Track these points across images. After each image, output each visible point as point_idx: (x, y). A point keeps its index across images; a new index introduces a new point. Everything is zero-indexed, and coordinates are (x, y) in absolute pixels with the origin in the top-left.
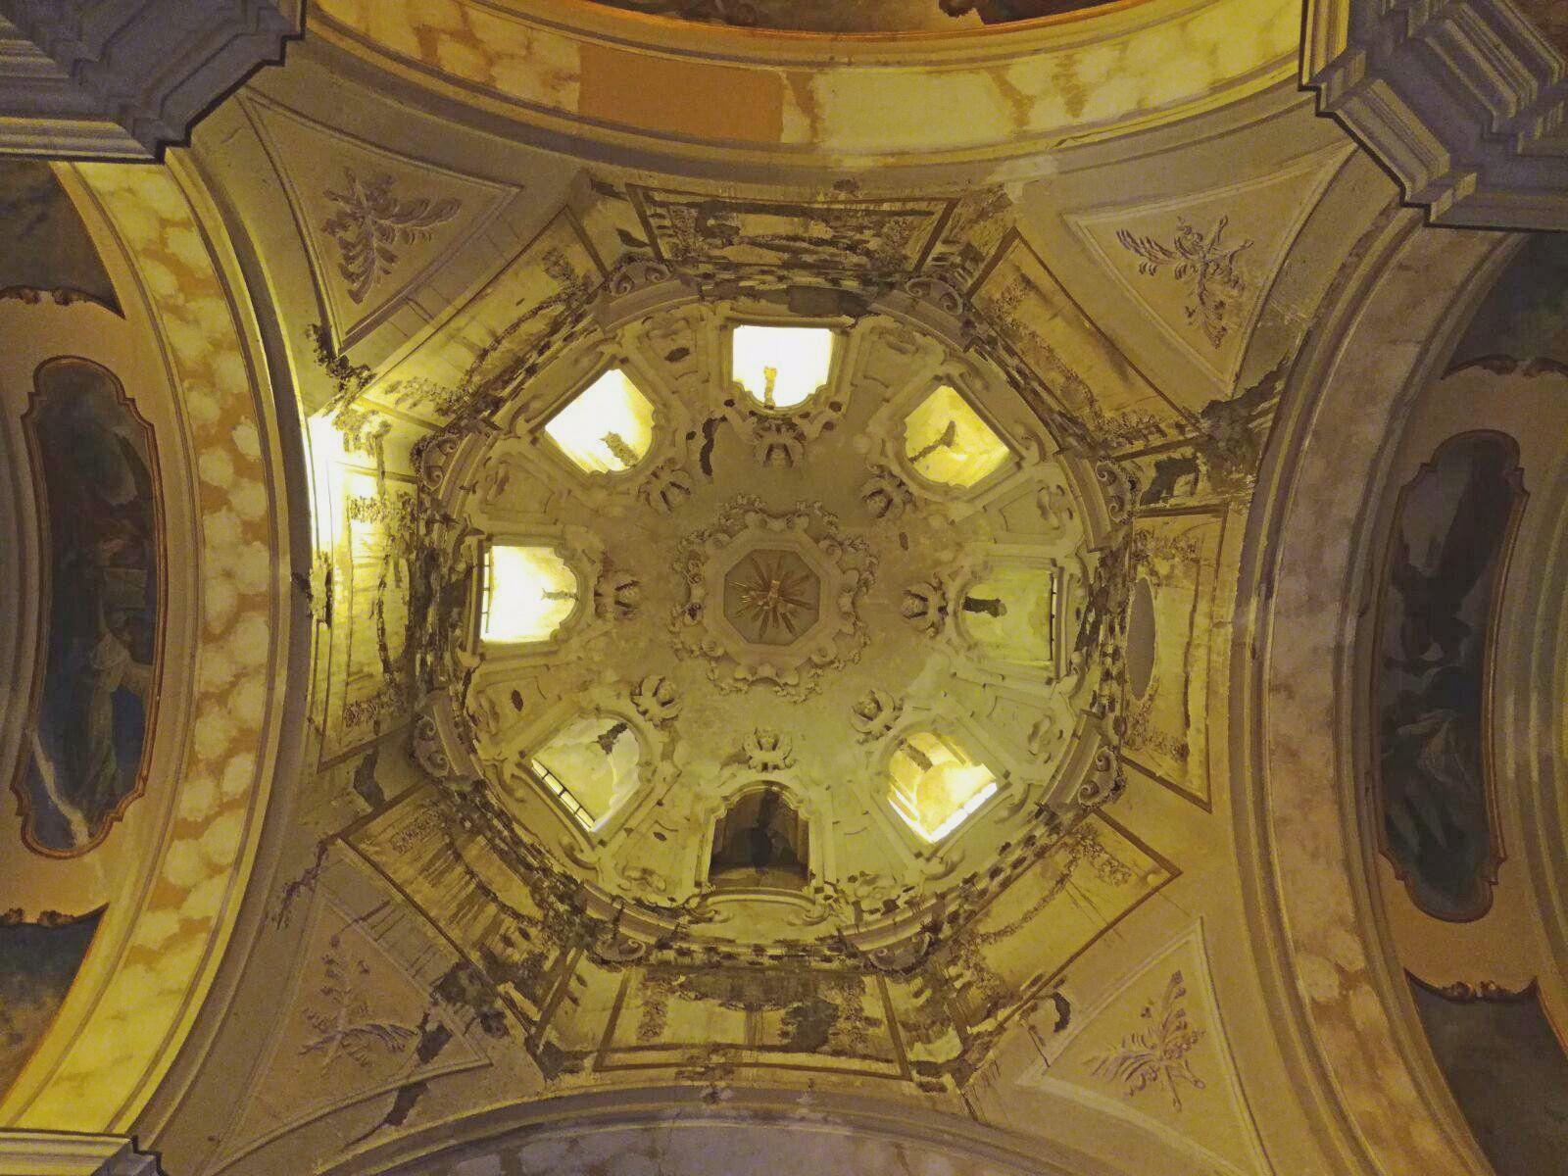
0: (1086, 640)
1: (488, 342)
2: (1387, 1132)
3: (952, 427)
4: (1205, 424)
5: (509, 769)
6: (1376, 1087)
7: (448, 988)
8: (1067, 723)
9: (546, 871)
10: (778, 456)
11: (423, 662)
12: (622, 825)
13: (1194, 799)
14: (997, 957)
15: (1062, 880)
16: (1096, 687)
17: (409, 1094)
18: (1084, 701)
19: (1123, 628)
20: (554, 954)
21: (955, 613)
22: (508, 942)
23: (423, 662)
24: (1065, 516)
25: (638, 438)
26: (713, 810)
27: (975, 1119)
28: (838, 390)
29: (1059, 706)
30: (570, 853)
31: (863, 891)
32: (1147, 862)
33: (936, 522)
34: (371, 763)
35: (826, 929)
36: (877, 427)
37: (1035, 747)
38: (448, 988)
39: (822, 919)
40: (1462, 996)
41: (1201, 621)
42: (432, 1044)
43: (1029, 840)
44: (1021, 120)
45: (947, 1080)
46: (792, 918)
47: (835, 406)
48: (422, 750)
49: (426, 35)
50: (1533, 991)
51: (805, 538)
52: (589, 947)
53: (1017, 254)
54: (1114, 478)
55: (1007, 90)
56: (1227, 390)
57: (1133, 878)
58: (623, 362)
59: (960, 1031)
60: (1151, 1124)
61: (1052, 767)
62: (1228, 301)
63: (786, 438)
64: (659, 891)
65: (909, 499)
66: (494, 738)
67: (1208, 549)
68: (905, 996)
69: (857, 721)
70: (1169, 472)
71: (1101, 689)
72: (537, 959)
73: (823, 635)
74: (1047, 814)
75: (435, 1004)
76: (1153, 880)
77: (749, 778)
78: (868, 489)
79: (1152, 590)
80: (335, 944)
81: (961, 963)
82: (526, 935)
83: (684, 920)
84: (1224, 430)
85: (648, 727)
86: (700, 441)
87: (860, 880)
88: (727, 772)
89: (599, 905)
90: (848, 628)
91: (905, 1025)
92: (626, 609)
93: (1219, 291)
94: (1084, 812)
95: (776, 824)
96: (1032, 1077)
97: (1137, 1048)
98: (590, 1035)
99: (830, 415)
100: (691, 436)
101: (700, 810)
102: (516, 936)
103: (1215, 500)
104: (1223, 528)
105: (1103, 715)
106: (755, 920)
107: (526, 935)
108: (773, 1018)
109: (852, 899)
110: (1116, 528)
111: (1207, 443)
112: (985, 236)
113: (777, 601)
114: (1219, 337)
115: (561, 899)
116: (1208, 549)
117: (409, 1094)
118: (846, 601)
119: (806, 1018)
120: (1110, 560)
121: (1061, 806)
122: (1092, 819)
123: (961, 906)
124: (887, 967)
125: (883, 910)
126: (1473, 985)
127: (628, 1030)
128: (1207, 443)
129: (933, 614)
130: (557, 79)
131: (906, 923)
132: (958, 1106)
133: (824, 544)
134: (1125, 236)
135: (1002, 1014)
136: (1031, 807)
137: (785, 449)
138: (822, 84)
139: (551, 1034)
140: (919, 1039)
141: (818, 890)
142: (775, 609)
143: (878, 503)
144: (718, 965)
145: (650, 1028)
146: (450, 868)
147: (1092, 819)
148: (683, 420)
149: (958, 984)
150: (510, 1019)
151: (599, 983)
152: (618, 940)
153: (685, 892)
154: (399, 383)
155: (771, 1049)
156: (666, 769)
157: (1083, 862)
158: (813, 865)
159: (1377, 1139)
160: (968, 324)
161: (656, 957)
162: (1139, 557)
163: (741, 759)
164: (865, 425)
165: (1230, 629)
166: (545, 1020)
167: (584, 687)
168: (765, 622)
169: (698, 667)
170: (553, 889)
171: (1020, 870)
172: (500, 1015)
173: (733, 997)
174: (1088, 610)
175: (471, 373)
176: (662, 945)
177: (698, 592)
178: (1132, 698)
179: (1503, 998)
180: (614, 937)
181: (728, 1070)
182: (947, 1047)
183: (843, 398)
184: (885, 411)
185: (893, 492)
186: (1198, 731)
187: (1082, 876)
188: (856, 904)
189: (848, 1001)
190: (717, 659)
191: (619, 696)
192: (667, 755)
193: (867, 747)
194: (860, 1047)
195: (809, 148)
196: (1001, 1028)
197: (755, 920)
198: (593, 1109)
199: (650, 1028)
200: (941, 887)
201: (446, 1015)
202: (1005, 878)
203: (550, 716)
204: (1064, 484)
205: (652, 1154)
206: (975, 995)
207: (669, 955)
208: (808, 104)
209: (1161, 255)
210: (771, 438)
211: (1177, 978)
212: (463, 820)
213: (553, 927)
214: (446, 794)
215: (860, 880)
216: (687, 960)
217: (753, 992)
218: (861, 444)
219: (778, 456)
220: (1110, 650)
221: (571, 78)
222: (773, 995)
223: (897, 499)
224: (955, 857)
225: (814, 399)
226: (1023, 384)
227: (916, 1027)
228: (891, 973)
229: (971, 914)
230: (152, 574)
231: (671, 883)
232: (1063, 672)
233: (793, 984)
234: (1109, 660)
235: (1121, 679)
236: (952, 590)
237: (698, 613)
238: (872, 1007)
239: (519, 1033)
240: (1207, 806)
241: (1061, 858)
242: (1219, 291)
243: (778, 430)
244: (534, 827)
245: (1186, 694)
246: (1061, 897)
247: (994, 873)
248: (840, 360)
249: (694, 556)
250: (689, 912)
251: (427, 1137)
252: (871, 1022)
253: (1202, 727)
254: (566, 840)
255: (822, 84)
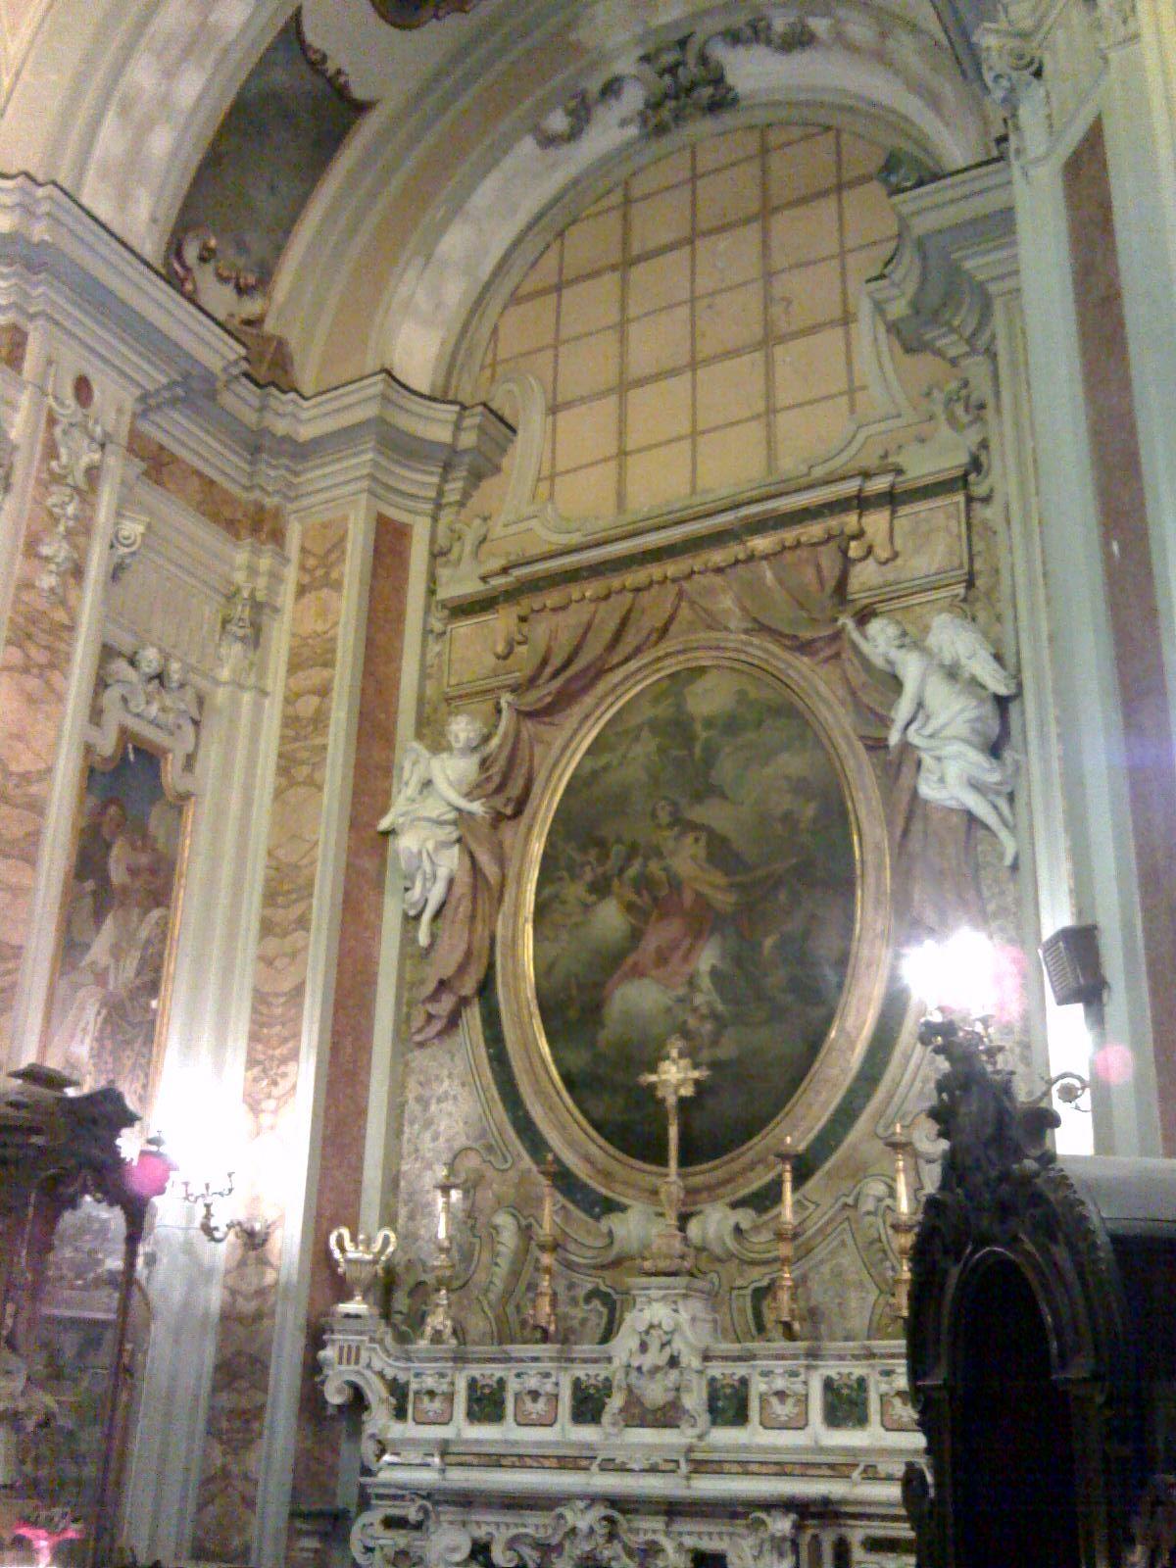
2: (137, 113)
6: (169, 74)
40: (316, 64)
50: (361, 108)
126: (331, 67)
154: (434, 882)
159: (125, 110)
179: (341, 93)
230: (581, 568)
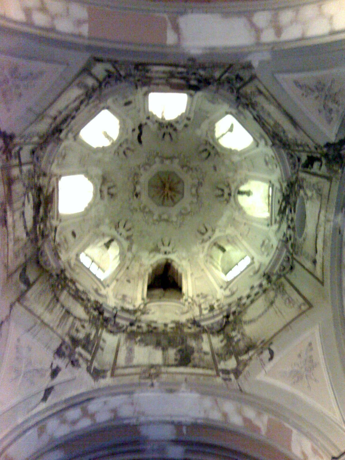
0: (282, 212)
1: (57, 114)
3: (232, 126)
4: (325, 150)
5: (73, 262)
7: (59, 353)
8: (275, 242)
9: (89, 300)
10: (167, 137)
11: (40, 228)
12: (114, 278)
13: (317, 278)
14: (249, 330)
15: (272, 303)
16: (285, 231)
17: (48, 391)
18: (280, 235)
19: (295, 211)
20: (94, 332)
21: (234, 196)
22: (77, 331)
23: (40, 228)
24: (275, 167)
25: (115, 134)
26: (147, 270)
27: (241, 390)
28: (189, 113)
29: (272, 235)
30: (96, 291)
31: (202, 301)
32: (301, 300)
33: (227, 162)
34: (24, 270)
35: (189, 316)
36: (204, 126)
37: (263, 249)
38: (59, 353)
39: (187, 312)
41: (322, 218)
42: (55, 373)
43: (261, 285)
44: (258, 38)
45: (232, 376)
46: (177, 311)
47: (188, 119)
48: (42, 260)
49: (28, 12)
51: (179, 168)
52: (106, 327)
53: (256, 82)
54: (292, 156)
55: (253, 25)
56: (333, 139)
57: (296, 306)
58: (108, 108)
59: (237, 358)
60: (301, 395)
61: (270, 258)
62: (334, 109)
63: (170, 130)
64: (129, 303)
65: (217, 153)
66: (67, 250)
67: (325, 191)
68: (218, 342)
69: (199, 235)
70: (311, 161)
71: (287, 231)
72: (88, 336)
73: (186, 202)
74: (268, 277)
75: (55, 358)
76: (303, 308)
77: (159, 258)
78: (201, 149)
79: (305, 201)
80: (18, 340)
81: (237, 331)
82: (83, 327)
83: (139, 313)
84: (331, 152)
85: (122, 240)
86: (137, 132)
87: (201, 296)
88: (152, 255)
89: (108, 312)
90: (195, 200)
91: (217, 354)
92: (112, 195)
93: (331, 105)
94: (279, 276)
95: (170, 273)
96: (261, 377)
97: (296, 368)
98: (109, 363)
99: (186, 122)
100: (134, 130)
101: (142, 269)
102: (80, 328)
103: (327, 174)
104: (330, 187)
105: (287, 241)
106: (164, 312)
107: (83, 327)
108: (172, 353)
109: (198, 303)
110: (292, 175)
111: (326, 156)
112: (245, 75)
113: (167, 189)
114: (330, 121)
115: (95, 309)
116: (325, 191)
117: (48, 391)
118: (194, 191)
119: (183, 352)
120: (291, 185)
121: (273, 274)
122: (283, 280)
123: (236, 308)
124: (212, 331)
125: (209, 308)
127: (122, 360)
128: (326, 156)
129: (226, 196)
130: (79, 23)
131: (217, 315)
132: (236, 386)
133: (185, 169)
134: (296, 83)
135: (251, 353)
136: (261, 272)
137: (170, 134)
138: (182, 21)
139: (95, 364)
140: (222, 359)
141: (186, 300)
142: (167, 194)
143: (205, 155)
144: (152, 332)
145: (129, 358)
146: (55, 306)
147: (283, 280)
148: (131, 124)
149: (236, 339)
150: (81, 361)
151: (110, 340)
152: (116, 324)
153: (139, 302)
155: (172, 366)
156: (129, 255)
157: (279, 296)
158: (184, 290)
160: (238, 98)
161: (129, 329)
162: (301, 187)
163: (156, 250)
164: (200, 125)
165: (332, 223)
166: (93, 359)
167: (98, 226)
168: (164, 199)
169: (138, 216)
170: (92, 306)
171: (257, 296)
172: (77, 361)
173: (158, 344)
174: (283, 201)
175: (51, 125)
176: (132, 324)
177: (138, 188)
178: (297, 238)
180: (115, 323)
181: (157, 375)
182: (231, 364)
183: (192, 116)
184: (207, 122)
185: (210, 150)
186: (320, 256)
187: (279, 301)
188: (200, 306)
189: (197, 345)
190: (147, 213)
191: (111, 228)
192: (130, 249)
193: (203, 245)
194: (202, 364)
195: (178, 45)
196: (250, 359)
197: (164, 312)
198: (111, 391)
199: (129, 358)
200: (230, 300)
201: (60, 362)
202: (252, 299)
203: (86, 238)
204: (274, 156)
205: (132, 404)
206: (242, 345)
207: (134, 328)
208: (176, 28)
209: (310, 91)
210: (164, 130)
211: (310, 344)
212: (58, 285)
213: (93, 321)
214: (51, 276)
215: (201, 296)
216: (140, 330)
217: (164, 342)
218: (198, 132)
219: (167, 137)
220: (290, 218)
221: (84, 22)
222: (171, 343)
223: (212, 153)
224: (235, 289)
225: (181, 117)
226: (258, 119)
227: (221, 355)
228: (213, 333)
229: (240, 313)
231: (134, 299)
232: (273, 222)
233: (178, 339)
234: (290, 222)
235: (294, 229)
236: (233, 187)
237: (139, 196)
238: (206, 347)
239: (84, 366)
240: (322, 283)
241: (272, 294)
242: (331, 105)
243: (167, 127)
244: (84, 284)
245: (316, 242)
246: (271, 310)
247: (248, 297)
248: (190, 104)
249: (136, 174)
250: (140, 310)
251: (55, 405)
252: (206, 353)
253: (322, 256)
254: (95, 287)
255: (182, 21)
